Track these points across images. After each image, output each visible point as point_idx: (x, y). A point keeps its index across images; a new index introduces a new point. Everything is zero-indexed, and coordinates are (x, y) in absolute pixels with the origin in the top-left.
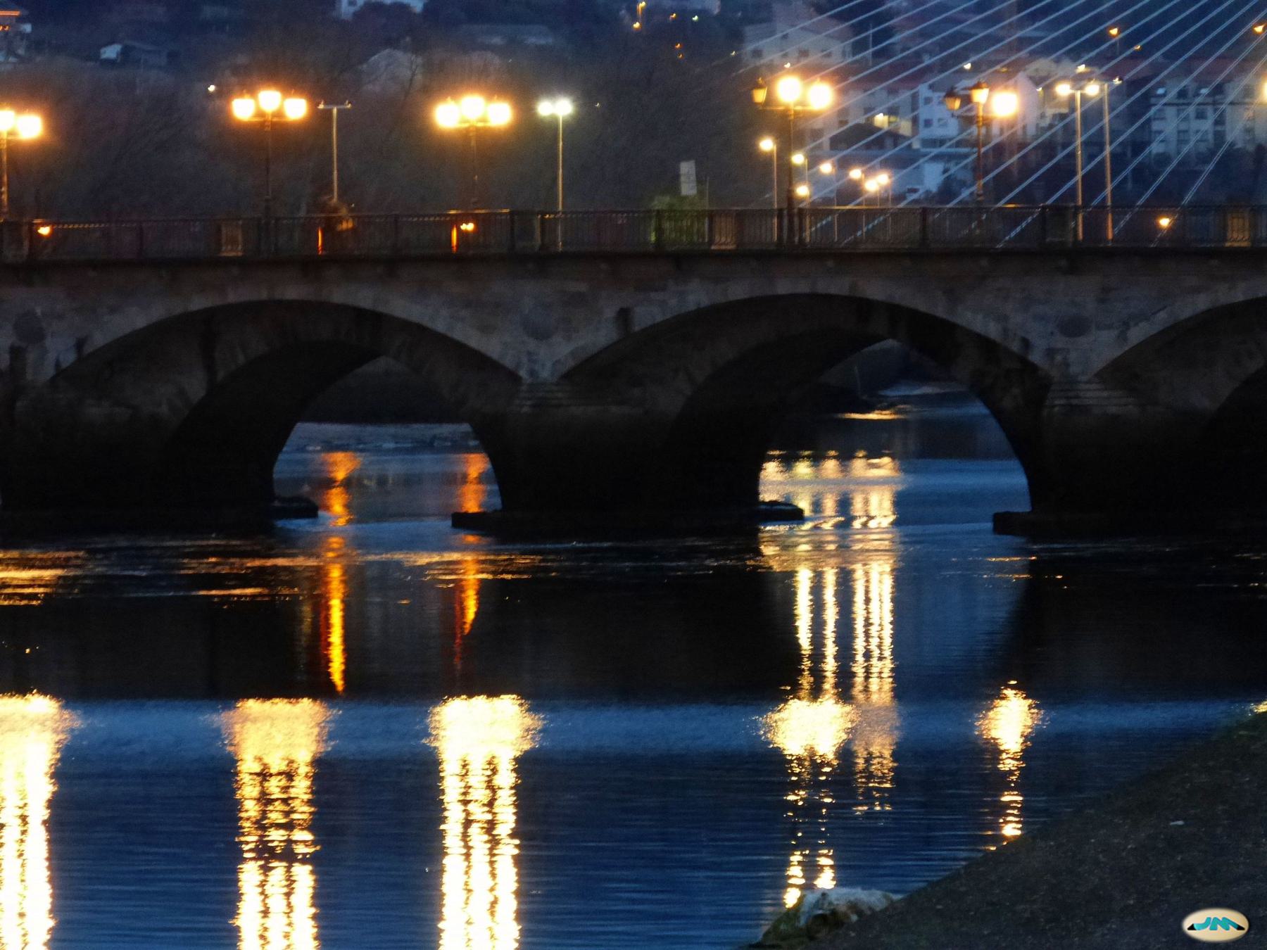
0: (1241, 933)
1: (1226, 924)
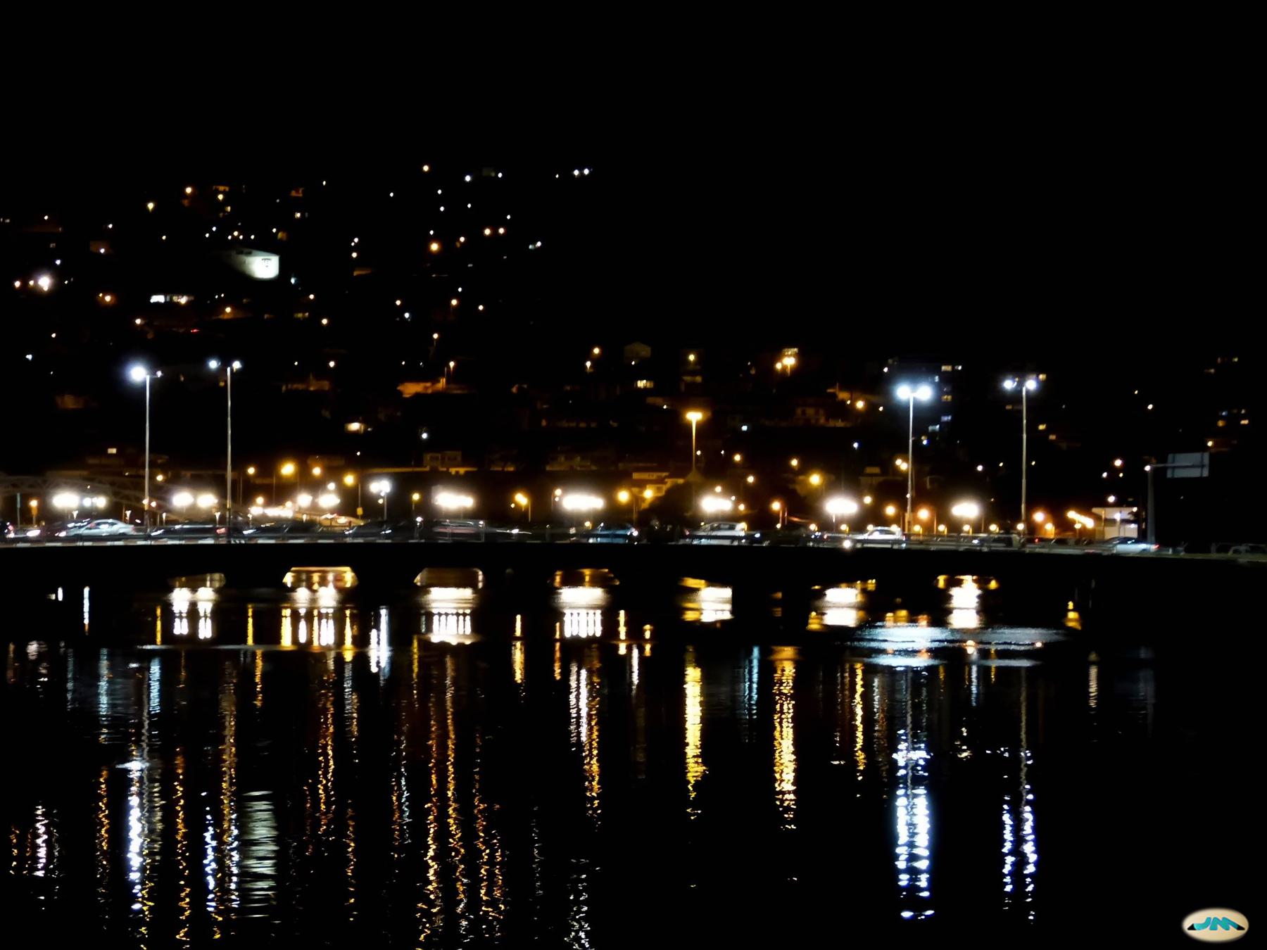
0: (1241, 933)
1: (1226, 924)
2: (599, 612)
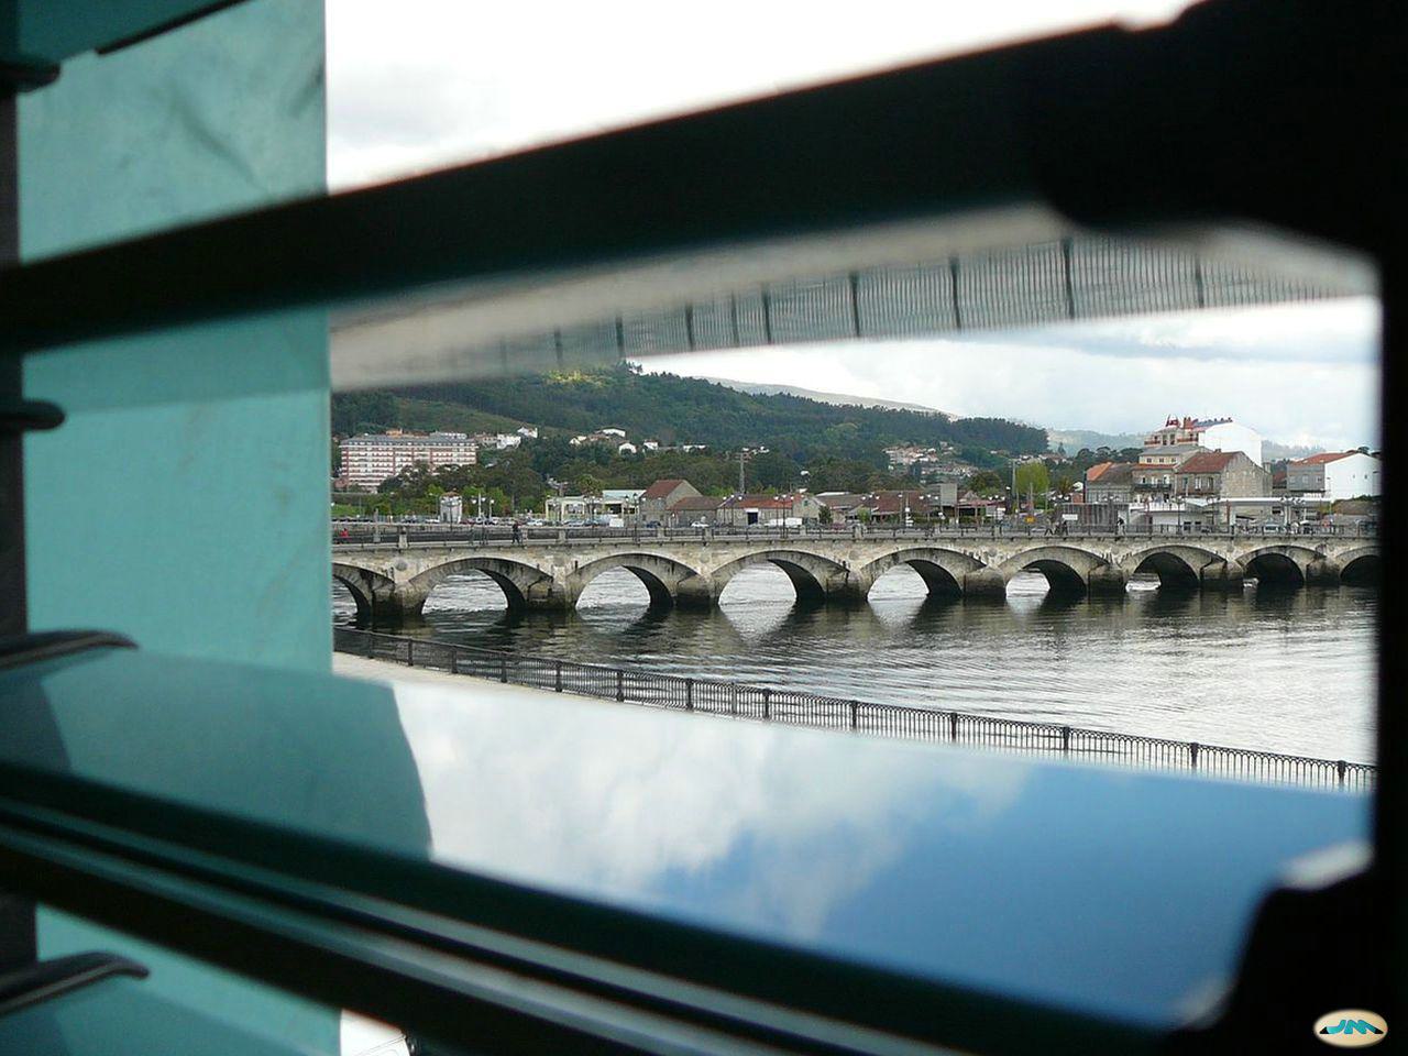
0: (1379, 1037)
1: (1362, 1027)
2: (41, 619)
